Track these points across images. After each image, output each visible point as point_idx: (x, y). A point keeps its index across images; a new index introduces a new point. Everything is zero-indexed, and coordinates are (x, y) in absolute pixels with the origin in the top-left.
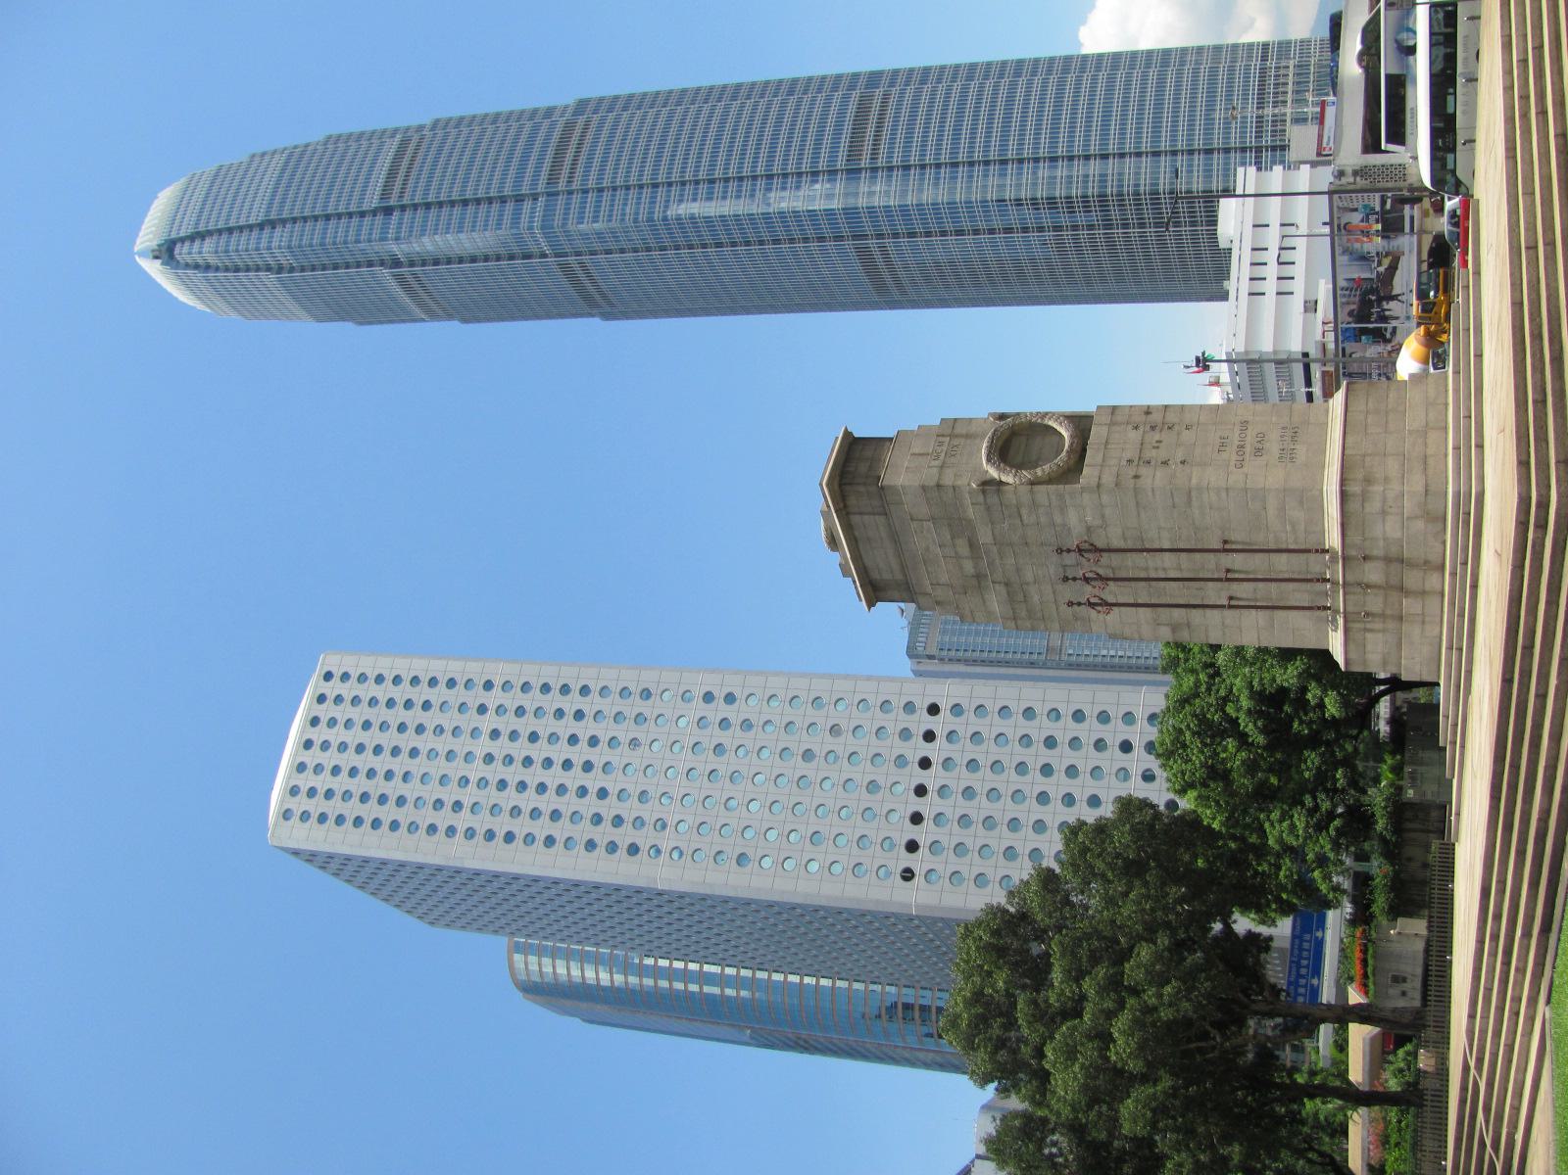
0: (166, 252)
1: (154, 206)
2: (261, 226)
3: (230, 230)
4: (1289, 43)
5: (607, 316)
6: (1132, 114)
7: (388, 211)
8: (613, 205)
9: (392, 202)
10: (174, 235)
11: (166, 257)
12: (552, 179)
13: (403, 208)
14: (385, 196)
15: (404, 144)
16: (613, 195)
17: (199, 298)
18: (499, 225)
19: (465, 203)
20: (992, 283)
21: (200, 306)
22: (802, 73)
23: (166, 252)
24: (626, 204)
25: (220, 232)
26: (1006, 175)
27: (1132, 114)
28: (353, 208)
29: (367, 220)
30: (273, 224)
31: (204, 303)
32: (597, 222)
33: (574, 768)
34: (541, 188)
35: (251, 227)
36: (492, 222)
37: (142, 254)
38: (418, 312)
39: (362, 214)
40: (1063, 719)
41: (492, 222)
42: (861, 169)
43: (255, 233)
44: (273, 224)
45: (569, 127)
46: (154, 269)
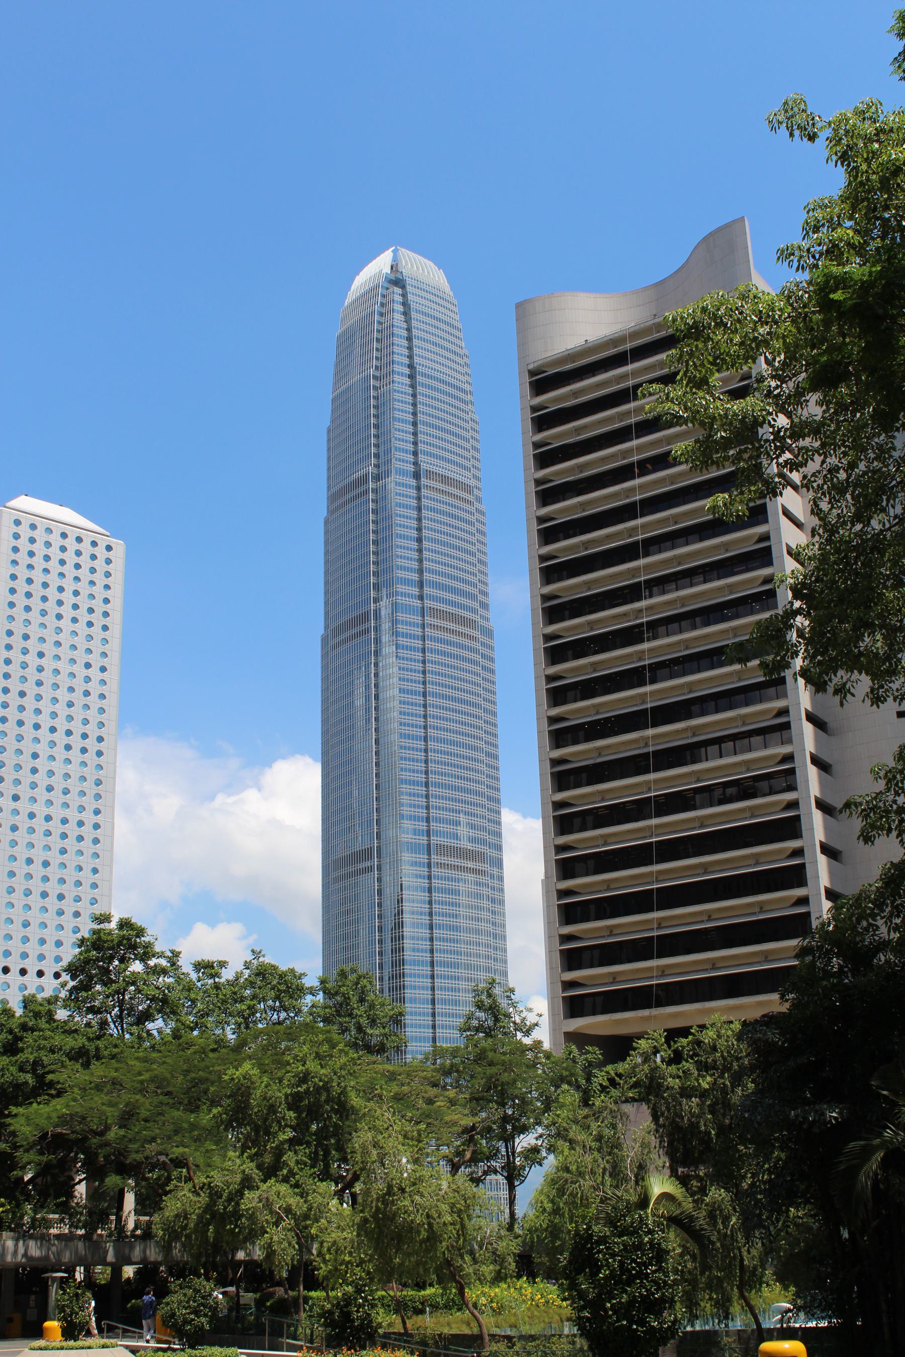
0: (397, 281)
1: (432, 265)
2: (411, 366)
3: (409, 339)
4: (505, 940)
5: (325, 640)
6: (458, 673)
7: (417, 475)
8: (409, 726)
9: (424, 481)
10: (409, 289)
11: (392, 277)
12: (435, 612)
13: (418, 488)
14: (429, 474)
15: (468, 489)
16: (418, 661)
17: (357, 299)
18: (403, 736)
19: (419, 540)
20: (345, 949)
21: (347, 301)
22: (502, 763)
23: (397, 281)
24: (410, 795)
25: (409, 330)
26: (415, 834)
27: (458, 673)
28: (421, 446)
29: (411, 458)
30: (412, 377)
31: (349, 306)
32: (400, 692)
33: (19, 714)
34: (428, 603)
35: (410, 357)
36: (407, 709)
37: (395, 259)
38: (333, 490)
39: (415, 454)
40: (7, 896)
41: (407, 709)
42: (424, 617)
43: (406, 361)
44: (412, 377)
45: (471, 623)
46: (381, 264)
